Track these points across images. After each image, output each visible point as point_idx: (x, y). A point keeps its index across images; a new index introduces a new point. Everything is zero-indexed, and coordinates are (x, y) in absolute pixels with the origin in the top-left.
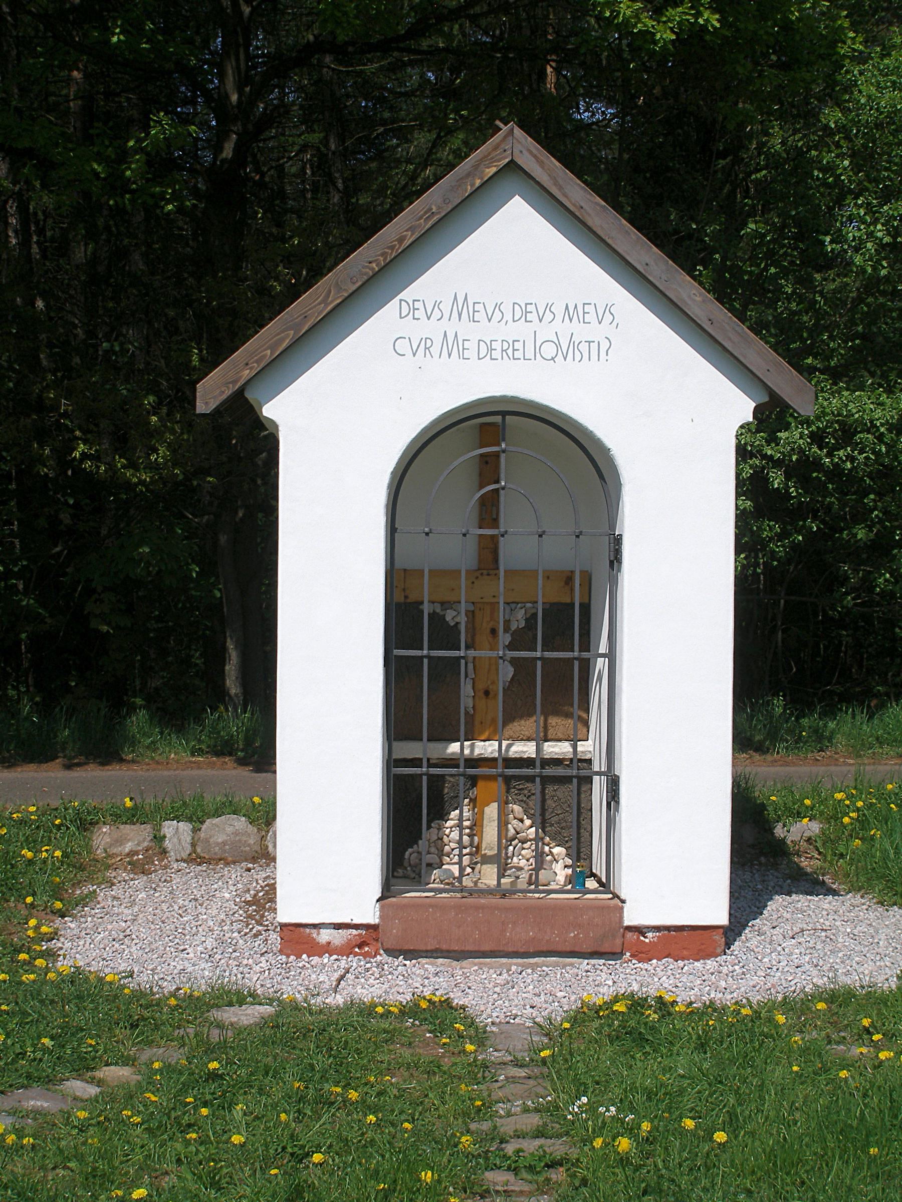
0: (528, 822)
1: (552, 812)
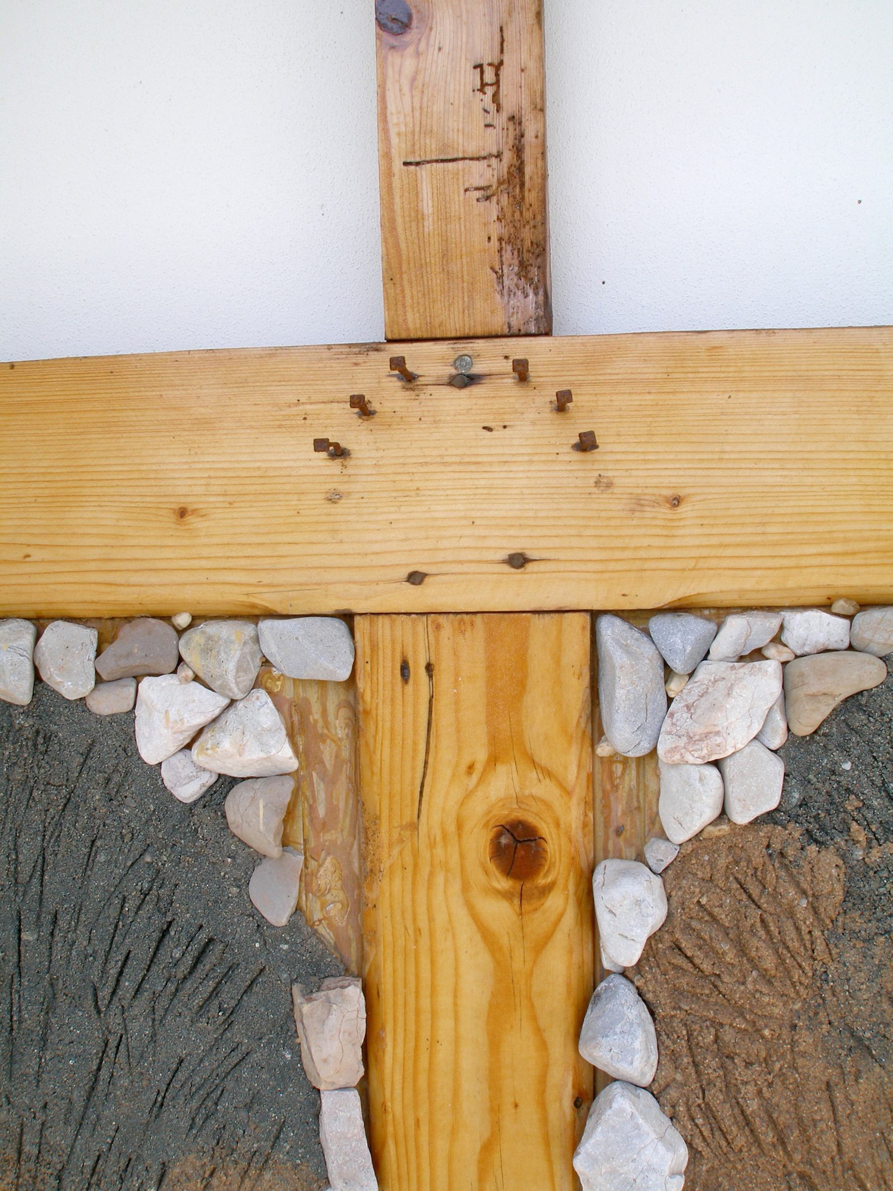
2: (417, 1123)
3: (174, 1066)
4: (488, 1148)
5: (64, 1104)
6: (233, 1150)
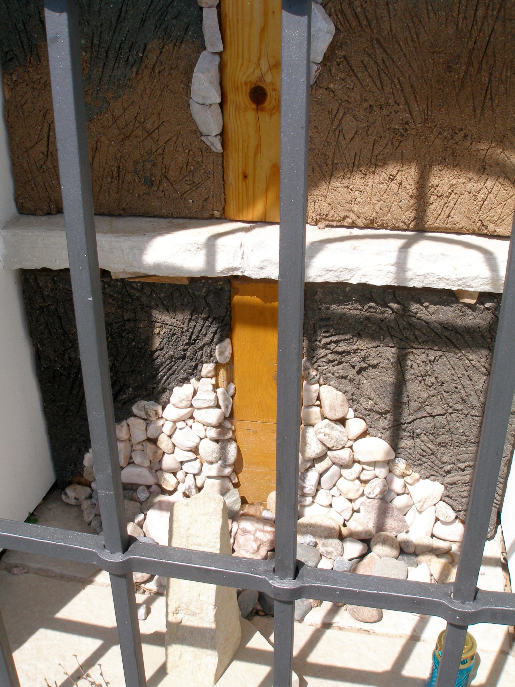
0: (356, 426)
1: (419, 409)
2: (238, 21)
3: (149, 3)
4: (263, 30)
5: (109, 22)
6: (171, 36)
